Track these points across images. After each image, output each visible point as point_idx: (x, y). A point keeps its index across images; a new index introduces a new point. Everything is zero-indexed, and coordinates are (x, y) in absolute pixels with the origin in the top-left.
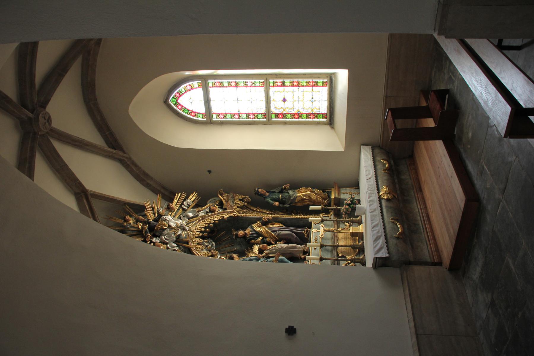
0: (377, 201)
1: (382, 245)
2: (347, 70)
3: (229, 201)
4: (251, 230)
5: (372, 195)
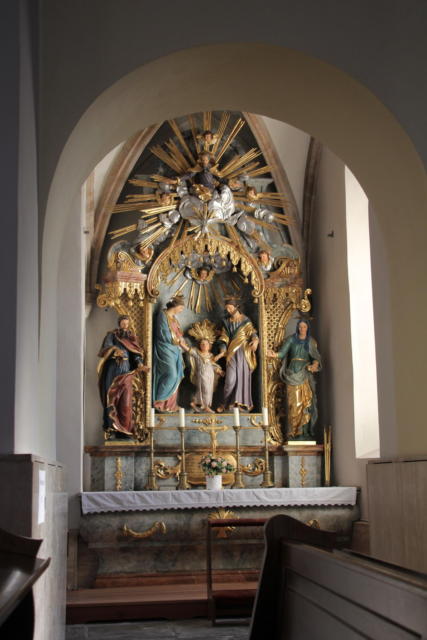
0: (199, 504)
1: (104, 505)
2: (379, 457)
3: (280, 280)
4: (239, 322)
5: (215, 499)
